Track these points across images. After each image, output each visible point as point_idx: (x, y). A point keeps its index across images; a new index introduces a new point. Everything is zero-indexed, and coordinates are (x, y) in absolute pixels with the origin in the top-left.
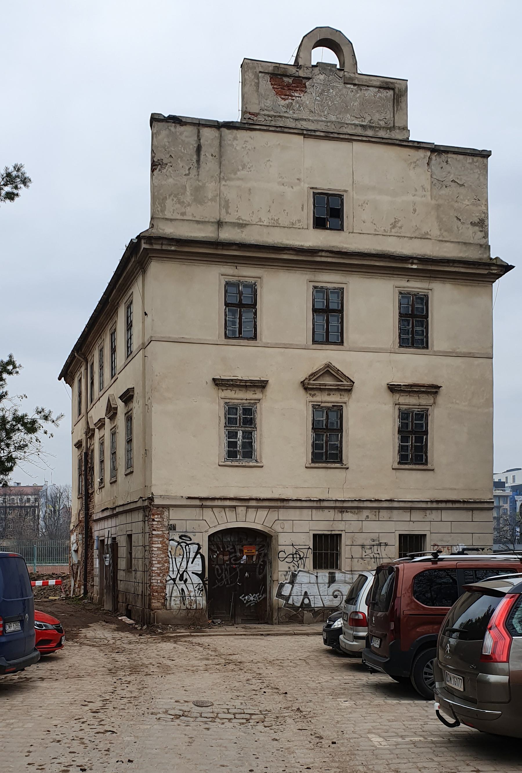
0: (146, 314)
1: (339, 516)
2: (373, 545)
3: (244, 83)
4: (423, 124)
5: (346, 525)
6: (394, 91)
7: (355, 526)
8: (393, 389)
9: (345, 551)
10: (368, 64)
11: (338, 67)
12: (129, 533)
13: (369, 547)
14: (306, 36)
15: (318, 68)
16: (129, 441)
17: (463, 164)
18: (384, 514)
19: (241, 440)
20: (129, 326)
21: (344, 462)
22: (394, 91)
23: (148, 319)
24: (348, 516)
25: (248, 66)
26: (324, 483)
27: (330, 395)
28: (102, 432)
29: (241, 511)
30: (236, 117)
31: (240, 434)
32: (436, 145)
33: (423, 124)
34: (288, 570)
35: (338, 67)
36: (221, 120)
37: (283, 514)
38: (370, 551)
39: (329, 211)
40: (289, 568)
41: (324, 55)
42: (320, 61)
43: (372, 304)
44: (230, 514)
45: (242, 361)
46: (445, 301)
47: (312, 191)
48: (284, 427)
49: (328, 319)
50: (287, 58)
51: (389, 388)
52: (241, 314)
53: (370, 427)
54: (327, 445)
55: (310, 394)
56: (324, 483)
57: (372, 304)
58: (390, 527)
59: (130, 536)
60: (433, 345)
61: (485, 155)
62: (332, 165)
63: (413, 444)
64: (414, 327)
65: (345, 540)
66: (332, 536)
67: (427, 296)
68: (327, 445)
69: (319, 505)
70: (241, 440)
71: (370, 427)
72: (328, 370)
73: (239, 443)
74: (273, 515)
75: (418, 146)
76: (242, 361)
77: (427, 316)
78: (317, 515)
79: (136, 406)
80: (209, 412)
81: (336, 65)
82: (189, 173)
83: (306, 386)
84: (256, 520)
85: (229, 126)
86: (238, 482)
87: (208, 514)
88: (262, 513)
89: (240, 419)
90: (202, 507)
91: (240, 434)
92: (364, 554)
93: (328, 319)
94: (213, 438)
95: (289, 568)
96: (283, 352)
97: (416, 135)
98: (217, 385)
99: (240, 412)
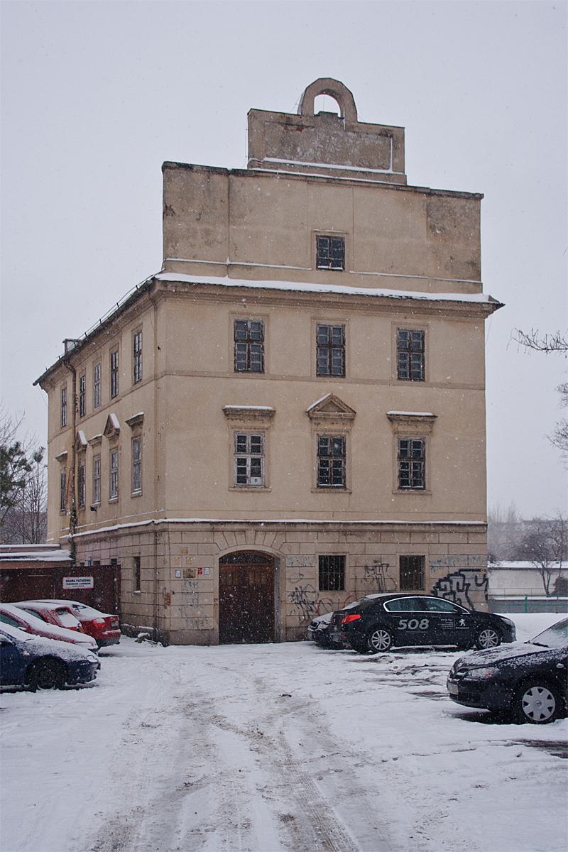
0: (159, 348)
1: (343, 539)
2: (376, 566)
3: (250, 130)
4: (421, 169)
5: (351, 548)
6: (392, 137)
7: (358, 548)
8: (392, 418)
9: (349, 572)
10: (367, 113)
11: (339, 116)
12: (137, 555)
13: (371, 568)
14: (309, 86)
15: (320, 117)
16: (137, 464)
17: (454, 212)
18: (385, 537)
19: (249, 461)
20: (137, 353)
21: (348, 487)
22: (392, 137)
23: (162, 354)
24: (351, 539)
25: (253, 114)
26: (329, 507)
27: (333, 424)
28: (97, 450)
29: (250, 534)
30: (243, 165)
31: (249, 462)
32: (431, 190)
33: (421, 169)
34: (295, 591)
35: (339, 116)
36: (230, 168)
37: (291, 537)
38: (373, 572)
39: (331, 252)
40: (296, 589)
41: (325, 104)
42: (322, 110)
43: (371, 344)
44: (240, 538)
45: (250, 393)
46: (441, 341)
47: (315, 234)
48: (292, 453)
49: (331, 353)
50: (292, 109)
51: (389, 418)
52: (249, 351)
53: (372, 458)
54: (331, 470)
55: (315, 424)
56: (329, 507)
57: (371, 344)
58: (391, 548)
59: (137, 559)
60: (428, 379)
61: (478, 197)
62: (333, 210)
63: (412, 469)
64: (411, 358)
65: (349, 563)
66: (337, 557)
67: (423, 332)
68: (331, 470)
69: (323, 527)
70: (249, 461)
71: (372, 458)
72: (333, 403)
73: (248, 469)
74: (281, 539)
75: (415, 190)
76: (250, 393)
77: (423, 351)
78: (324, 537)
79: (147, 431)
80: (221, 439)
81: (337, 114)
82: (200, 217)
83: (310, 415)
84: (264, 544)
85: (236, 172)
86: (244, 506)
87: (219, 538)
88: (271, 536)
89: (249, 447)
90: (213, 531)
91: (249, 462)
92: (367, 575)
93: (331, 353)
94: (225, 466)
95: (296, 589)
96: (289, 385)
97: (411, 182)
98: (227, 415)
99: (249, 440)
